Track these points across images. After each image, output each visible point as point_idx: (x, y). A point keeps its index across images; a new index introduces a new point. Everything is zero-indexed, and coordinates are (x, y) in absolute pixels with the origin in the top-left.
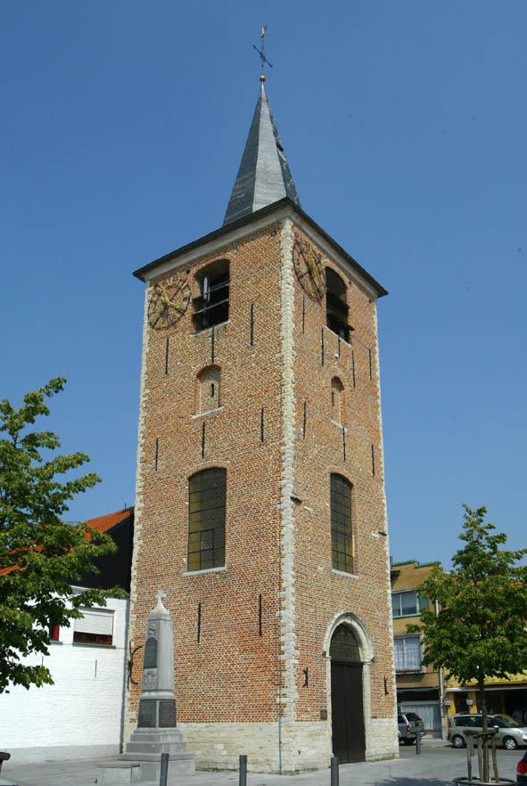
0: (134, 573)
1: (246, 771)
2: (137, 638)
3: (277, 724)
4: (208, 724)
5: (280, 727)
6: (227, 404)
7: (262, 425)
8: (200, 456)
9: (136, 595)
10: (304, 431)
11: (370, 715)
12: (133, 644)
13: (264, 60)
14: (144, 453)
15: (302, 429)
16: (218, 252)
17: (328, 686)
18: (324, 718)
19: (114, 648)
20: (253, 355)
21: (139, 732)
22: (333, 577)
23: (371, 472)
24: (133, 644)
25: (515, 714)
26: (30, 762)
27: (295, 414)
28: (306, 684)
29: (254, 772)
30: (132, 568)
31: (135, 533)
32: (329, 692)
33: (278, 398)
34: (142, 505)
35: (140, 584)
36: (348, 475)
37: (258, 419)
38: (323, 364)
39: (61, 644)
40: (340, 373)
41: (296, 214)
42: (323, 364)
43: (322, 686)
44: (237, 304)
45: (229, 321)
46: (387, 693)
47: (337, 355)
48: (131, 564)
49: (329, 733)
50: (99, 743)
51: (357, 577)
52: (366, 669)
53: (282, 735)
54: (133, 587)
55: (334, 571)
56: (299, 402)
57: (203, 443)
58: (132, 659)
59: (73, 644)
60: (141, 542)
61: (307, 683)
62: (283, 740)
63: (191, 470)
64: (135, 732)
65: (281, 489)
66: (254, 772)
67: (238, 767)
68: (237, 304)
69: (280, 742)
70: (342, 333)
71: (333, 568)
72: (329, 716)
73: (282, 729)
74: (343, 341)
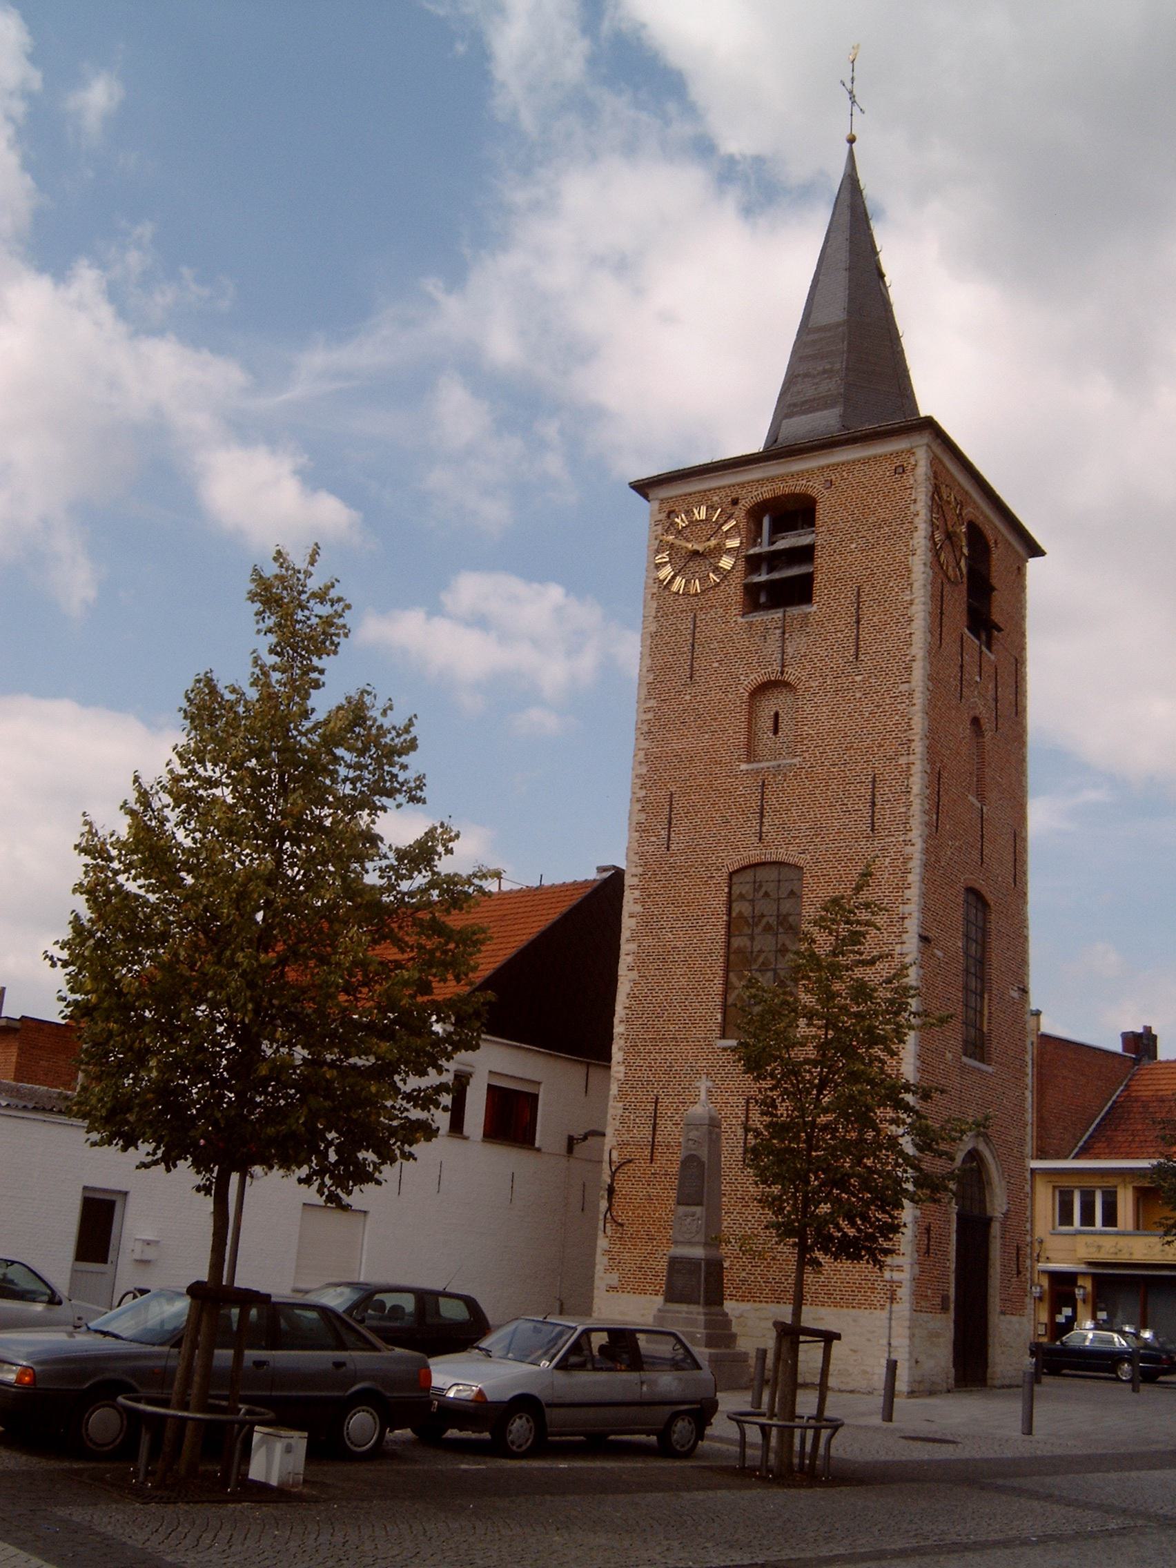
0: (619, 1029)
1: (827, 1388)
2: (622, 1145)
3: (885, 1314)
4: (757, 1305)
5: (890, 1319)
6: (806, 755)
7: (873, 804)
8: (755, 839)
9: (622, 1068)
10: (937, 820)
11: (998, 1309)
12: (615, 1154)
13: (851, 92)
14: (644, 816)
15: (935, 817)
16: (800, 474)
17: (953, 1255)
18: (945, 1309)
19: (466, 1138)
20: (858, 678)
21: (668, 1311)
22: (963, 1068)
23: (1011, 881)
24: (615, 1154)
25: (408, 1303)
26: (990, 1350)
27: (928, 791)
28: (928, 1252)
29: (841, 1391)
30: (616, 1021)
31: (622, 957)
32: (953, 1266)
33: (903, 760)
34: (638, 908)
35: (632, 1049)
36: (985, 891)
37: (865, 791)
38: (961, 697)
39: (466, 1138)
40: (984, 713)
41: (939, 441)
42: (961, 697)
43: (946, 1253)
44: (829, 580)
45: (815, 608)
46: (1019, 1273)
47: (978, 680)
48: (612, 1013)
49: (949, 1334)
50: (453, 1317)
51: (990, 1069)
52: (996, 1229)
53: (894, 1333)
54: (617, 1055)
55: (965, 1059)
56: (933, 769)
57: (762, 816)
58: (613, 1180)
59: (483, 1141)
60: (634, 975)
61: (928, 1249)
62: (894, 1343)
63: (735, 861)
64: (659, 1310)
65: (903, 918)
66: (841, 1391)
67: (817, 1380)
68: (829, 580)
69: (890, 1344)
70: (984, 637)
71: (965, 1055)
72: (952, 1306)
73: (894, 1323)
74: (984, 648)
